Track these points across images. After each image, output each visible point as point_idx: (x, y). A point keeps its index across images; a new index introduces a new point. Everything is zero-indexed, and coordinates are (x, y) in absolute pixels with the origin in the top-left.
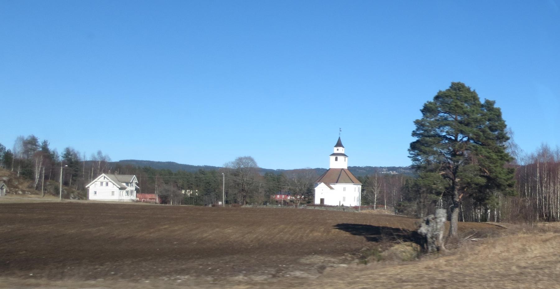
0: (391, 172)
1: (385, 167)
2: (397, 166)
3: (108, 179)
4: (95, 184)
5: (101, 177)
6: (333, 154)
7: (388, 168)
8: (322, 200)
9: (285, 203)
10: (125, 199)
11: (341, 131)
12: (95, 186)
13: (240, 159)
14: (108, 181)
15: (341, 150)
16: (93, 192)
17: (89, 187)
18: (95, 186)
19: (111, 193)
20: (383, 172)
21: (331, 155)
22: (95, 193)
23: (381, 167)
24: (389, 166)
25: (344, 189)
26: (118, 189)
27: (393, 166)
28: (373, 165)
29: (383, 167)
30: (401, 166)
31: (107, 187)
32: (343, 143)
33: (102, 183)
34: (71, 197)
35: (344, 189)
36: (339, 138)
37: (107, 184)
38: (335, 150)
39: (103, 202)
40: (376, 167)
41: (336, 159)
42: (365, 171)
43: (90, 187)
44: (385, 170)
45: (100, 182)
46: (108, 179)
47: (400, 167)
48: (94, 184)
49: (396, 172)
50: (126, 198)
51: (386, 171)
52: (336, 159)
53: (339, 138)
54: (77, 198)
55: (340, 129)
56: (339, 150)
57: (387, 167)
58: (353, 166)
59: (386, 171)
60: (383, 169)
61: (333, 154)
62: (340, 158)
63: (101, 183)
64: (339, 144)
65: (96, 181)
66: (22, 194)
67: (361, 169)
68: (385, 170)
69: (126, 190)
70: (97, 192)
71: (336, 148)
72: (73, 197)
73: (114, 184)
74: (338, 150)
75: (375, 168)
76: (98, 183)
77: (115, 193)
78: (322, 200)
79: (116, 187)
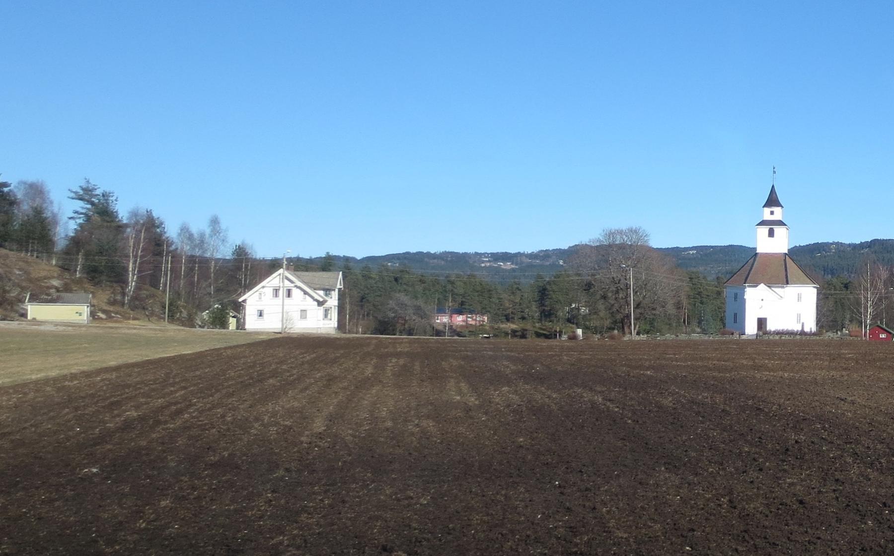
0: (502, 264)
1: (486, 253)
2: (513, 250)
3: (292, 282)
4: (260, 294)
5: (275, 277)
6: (763, 223)
7: (493, 254)
8: (762, 323)
9: (454, 331)
10: (321, 326)
11: (774, 172)
12: (260, 298)
13: (611, 234)
14: (293, 285)
15: (778, 213)
16: (265, 316)
17: (244, 301)
18: (260, 298)
19: (299, 312)
20: (483, 265)
21: (758, 225)
22: (261, 314)
23: (477, 254)
24: (495, 251)
25: (799, 298)
26: (316, 303)
27: (504, 251)
28: (460, 249)
29: (480, 255)
30: (522, 252)
31: (287, 300)
32: (781, 200)
33: (276, 291)
34: (198, 324)
35: (799, 298)
36: (773, 186)
37: (289, 293)
38: (766, 214)
39: (316, 336)
40: (466, 253)
41: (771, 234)
42: (443, 263)
43: (247, 301)
44: (487, 259)
45: (272, 289)
46: (292, 282)
47: (519, 253)
48: (258, 293)
49: (512, 264)
50: (324, 324)
51: (489, 261)
52: (771, 234)
53: (773, 186)
54: (206, 327)
55: (774, 168)
56: (775, 213)
57: (491, 253)
58: (415, 252)
59: (489, 261)
60: (481, 257)
61: (763, 223)
62: (778, 230)
63: (274, 289)
64: (772, 201)
65: (263, 287)
66: (106, 319)
67: (434, 258)
68: (487, 259)
69: (324, 306)
70: (265, 312)
71: (767, 210)
72: (200, 323)
73: (305, 293)
74: (772, 213)
75: (465, 255)
76: (269, 292)
77: (308, 312)
78: (762, 323)
79: (312, 300)
